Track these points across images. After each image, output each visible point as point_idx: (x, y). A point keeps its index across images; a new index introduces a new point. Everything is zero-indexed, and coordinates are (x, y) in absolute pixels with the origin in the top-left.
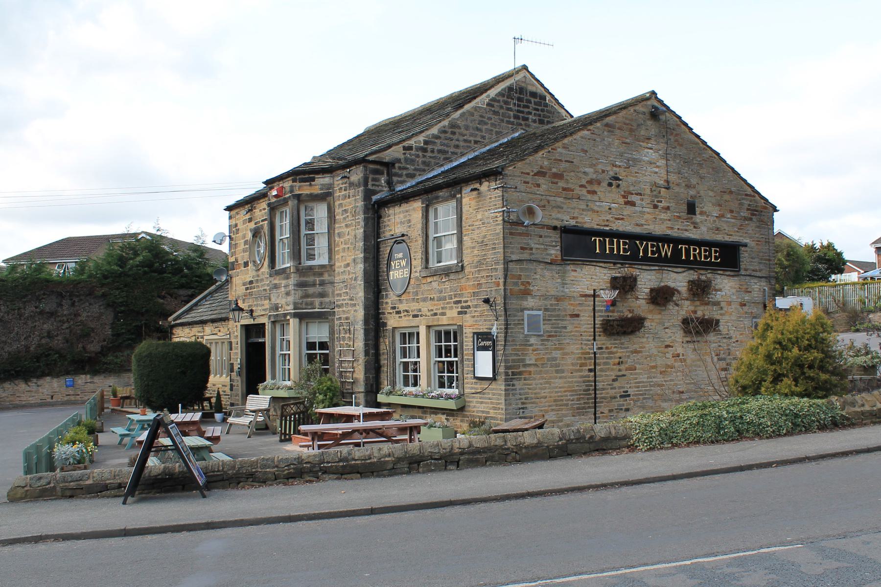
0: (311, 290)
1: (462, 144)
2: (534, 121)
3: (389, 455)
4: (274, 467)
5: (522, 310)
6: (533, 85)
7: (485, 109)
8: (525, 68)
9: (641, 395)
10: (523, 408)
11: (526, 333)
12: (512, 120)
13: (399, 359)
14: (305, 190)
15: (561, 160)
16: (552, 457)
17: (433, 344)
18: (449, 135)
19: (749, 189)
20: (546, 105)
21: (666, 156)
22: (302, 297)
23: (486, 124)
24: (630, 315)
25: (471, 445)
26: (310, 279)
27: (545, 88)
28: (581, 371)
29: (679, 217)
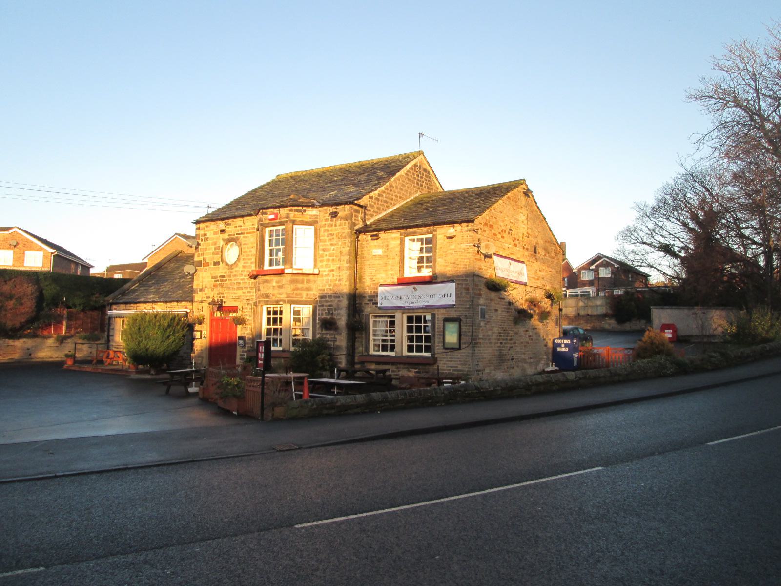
0: (300, 286)
17: (405, 324)
18: (389, 191)
20: (430, 178)
22: (294, 290)
24: (35, 313)
27: (430, 167)
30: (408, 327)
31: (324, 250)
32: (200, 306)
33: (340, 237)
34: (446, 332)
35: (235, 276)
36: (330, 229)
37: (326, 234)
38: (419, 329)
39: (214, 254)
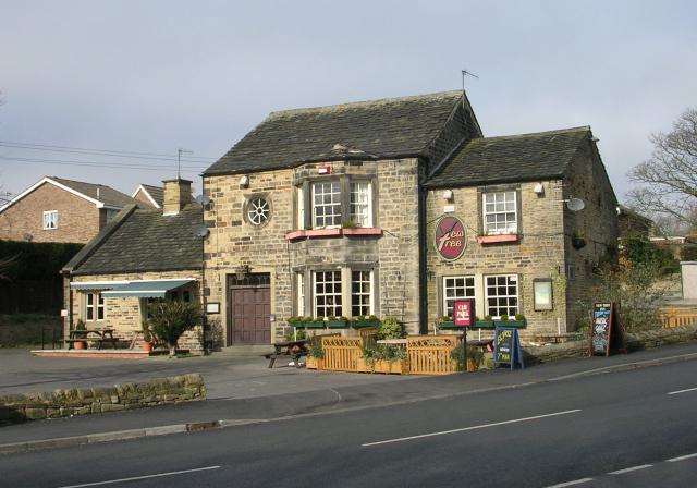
22: (353, 252)
30: (317, 286)
31: (385, 207)
32: (215, 273)
33: (406, 192)
34: (536, 293)
35: (266, 237)
36: (392, 184)
37: (387, 189)
38: (502, 291)
39: (232, 212)
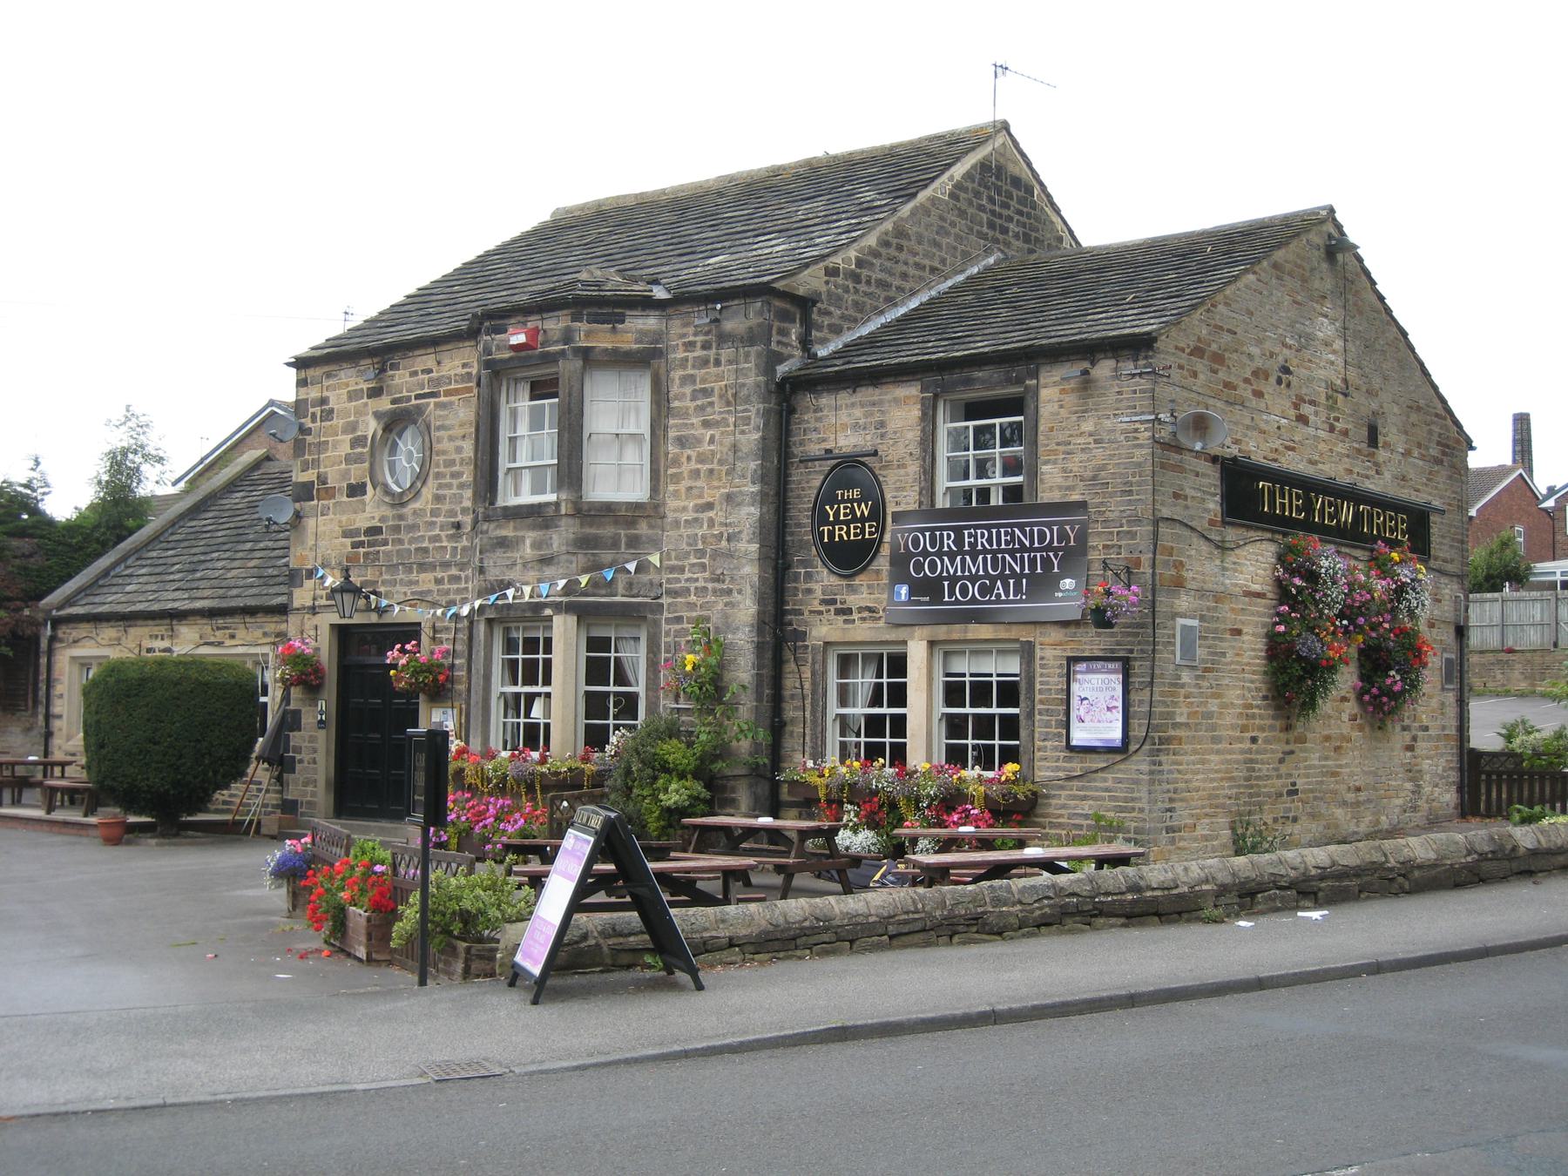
1: (912, 271)
2: (1017, 236)
3: (1207, 881)
4: (1014, 905)
5: (1174, 615)
6: (1016, 163)
7: (947, 204)
8: (1005, 127)
9: (1312, 791)
10: (1169, 810)
11: (1178, 660)
12: (985, 229)
13: (834, 709)
14: (603, 339)
15: (1221, 328)
16: (1458, 885)
18: (893, 252)
19: (1440, 406)
20: (1034, 206)
21: (1344, 333)
23: (948, 234)
25: (1334, 863)
26: (607, 531)
28: (1240, 740)
29: (1359, 451)
